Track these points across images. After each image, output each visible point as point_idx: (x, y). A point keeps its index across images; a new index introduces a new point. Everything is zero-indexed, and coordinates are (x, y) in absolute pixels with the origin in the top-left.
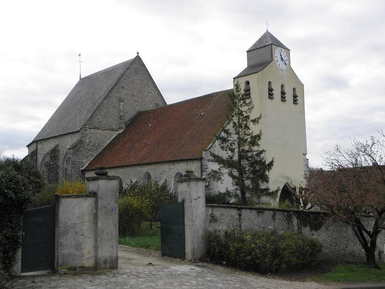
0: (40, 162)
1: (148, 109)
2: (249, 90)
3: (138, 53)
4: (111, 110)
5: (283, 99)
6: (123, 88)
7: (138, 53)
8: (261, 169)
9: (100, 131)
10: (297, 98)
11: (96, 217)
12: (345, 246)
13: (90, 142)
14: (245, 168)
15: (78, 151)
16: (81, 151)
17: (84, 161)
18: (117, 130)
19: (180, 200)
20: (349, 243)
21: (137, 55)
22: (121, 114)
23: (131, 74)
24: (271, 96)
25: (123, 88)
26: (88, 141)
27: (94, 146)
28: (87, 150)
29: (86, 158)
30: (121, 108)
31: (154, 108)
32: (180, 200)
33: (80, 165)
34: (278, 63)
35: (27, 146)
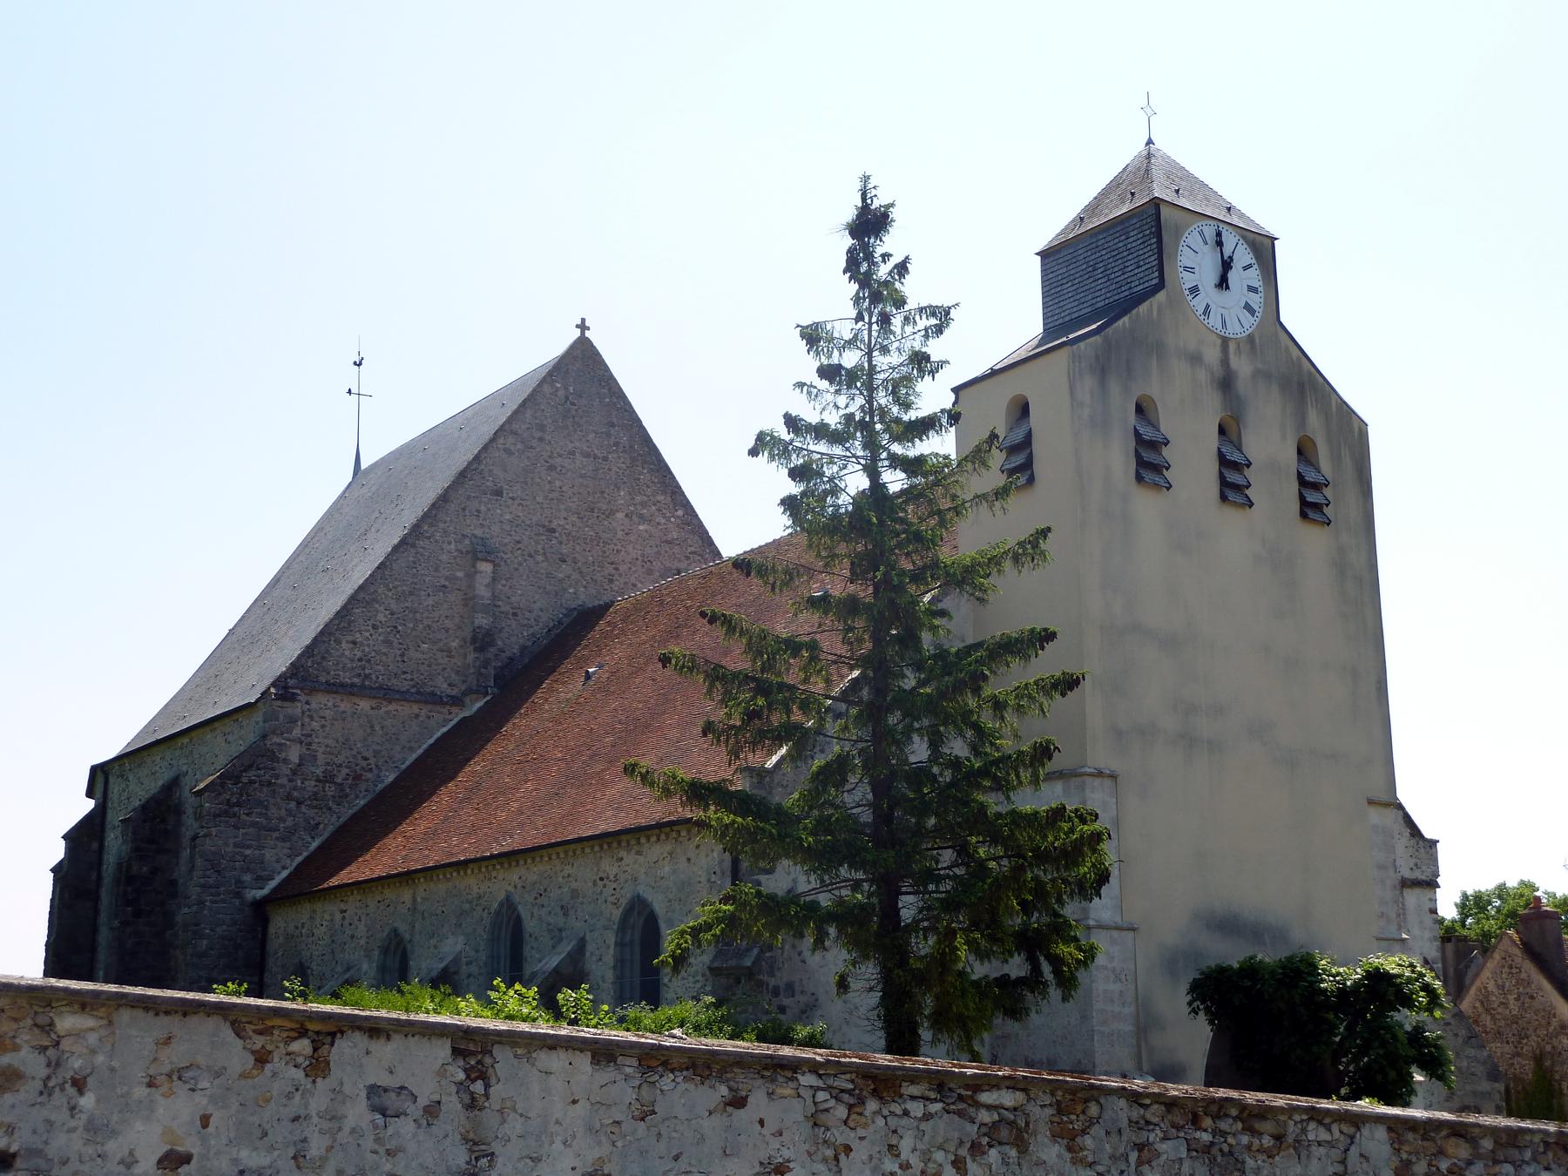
0: (111, 870)
2: (1027, 442)
3: (583, 326)
4: (430, 601)
5: (1232, 483)
6: (499, 493)
7: (583, 326)
9: (364, 705)
10: (1165, 451)
14: (840, 902)
15: (238, 804)
16: (260, 803)
17: (269, 855)
18: (457, 701)
21: (578, 333)
22: (482, 621)
23: (542, 428)
24: (1150, 462)
25: (499, 493)
26: (294, 754)
27: (328, 778)
28: (289, 797)
30: (482, 591)
33: (247, 878)
34: (1198, 304)
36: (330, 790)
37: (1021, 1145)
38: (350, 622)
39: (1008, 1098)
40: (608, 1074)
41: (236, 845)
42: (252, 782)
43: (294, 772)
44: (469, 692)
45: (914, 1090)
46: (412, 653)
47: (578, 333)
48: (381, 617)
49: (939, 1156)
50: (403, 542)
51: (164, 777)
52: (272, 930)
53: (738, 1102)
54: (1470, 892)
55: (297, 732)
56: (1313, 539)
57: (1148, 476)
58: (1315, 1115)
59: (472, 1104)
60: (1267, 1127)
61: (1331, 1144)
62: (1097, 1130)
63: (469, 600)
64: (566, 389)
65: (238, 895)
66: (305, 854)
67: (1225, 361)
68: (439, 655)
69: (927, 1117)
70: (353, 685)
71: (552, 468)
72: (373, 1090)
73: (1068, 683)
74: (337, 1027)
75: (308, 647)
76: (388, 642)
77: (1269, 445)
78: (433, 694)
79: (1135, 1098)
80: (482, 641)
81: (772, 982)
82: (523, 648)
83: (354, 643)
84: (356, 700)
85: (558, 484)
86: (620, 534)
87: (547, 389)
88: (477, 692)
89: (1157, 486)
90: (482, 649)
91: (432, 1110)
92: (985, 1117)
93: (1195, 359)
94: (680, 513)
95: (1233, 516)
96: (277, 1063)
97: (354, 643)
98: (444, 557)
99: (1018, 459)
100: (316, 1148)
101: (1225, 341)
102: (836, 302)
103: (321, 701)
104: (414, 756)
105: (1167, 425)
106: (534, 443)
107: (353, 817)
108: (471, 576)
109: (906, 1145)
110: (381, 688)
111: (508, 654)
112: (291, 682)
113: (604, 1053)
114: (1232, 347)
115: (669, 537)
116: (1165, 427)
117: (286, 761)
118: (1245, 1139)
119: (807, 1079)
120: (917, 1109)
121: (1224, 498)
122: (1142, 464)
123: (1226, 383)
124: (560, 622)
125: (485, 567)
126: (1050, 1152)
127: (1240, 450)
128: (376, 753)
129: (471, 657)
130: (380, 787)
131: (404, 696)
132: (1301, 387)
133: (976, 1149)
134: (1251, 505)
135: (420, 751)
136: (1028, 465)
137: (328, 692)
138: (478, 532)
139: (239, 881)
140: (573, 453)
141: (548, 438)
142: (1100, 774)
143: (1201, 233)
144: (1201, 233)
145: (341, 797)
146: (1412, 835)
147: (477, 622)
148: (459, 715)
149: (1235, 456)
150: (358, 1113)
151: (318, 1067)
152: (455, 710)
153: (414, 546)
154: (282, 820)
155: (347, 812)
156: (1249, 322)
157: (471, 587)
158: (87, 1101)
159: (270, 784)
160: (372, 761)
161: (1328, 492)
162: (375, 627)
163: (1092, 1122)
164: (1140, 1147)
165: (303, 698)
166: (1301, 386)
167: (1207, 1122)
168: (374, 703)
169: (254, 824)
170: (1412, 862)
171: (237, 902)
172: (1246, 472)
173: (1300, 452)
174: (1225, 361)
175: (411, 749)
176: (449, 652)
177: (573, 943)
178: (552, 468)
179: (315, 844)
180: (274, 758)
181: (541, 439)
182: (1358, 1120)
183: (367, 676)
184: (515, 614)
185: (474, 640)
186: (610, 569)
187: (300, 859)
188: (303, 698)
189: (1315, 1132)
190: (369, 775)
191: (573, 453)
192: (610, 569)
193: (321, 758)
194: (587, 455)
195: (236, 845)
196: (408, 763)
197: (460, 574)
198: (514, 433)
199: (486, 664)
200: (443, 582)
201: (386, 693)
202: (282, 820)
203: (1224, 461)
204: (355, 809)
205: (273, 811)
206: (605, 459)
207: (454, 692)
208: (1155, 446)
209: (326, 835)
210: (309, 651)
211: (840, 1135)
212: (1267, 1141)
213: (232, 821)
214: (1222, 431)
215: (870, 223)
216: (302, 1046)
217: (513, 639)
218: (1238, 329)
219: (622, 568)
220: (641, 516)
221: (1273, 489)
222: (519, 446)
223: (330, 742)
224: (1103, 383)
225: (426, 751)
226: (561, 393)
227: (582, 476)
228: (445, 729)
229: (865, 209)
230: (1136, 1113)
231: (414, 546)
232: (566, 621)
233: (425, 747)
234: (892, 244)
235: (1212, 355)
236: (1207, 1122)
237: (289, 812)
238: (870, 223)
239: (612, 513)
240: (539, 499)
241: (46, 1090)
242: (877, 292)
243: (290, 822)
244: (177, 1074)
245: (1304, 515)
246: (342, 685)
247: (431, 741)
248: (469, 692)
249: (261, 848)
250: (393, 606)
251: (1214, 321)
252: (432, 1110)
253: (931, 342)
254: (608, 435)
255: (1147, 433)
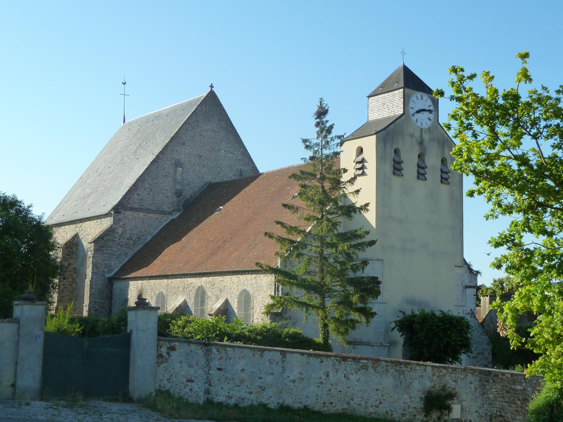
1: (226, 179)
3: (212, 86)
4: (162, 180)
5: (421, 175)
6: (184, 144)
7: (212, 86)
8: (370, 287)
9: (142, 214)
10: (402, 165)
11: (17, 344)
12: (378, 402)
13: (124, 232)
15: (103, 247)
16: (110, 246)
17: (113, 263)
18: (170, 213)
19: (128, 331)
20: (385, 398)
22: (179, 187)
25: (184, 144)
28: (119, 245)
29: (117, 258)
30: (179, 177)
31: (234, 178)
32: (128, 331)
33: (106, 270)
35: (406, 70)
36: (131, 242)
37: (367, 369)
38: (137, 187)
39: (365, 361)
40: (303, 357)
41: (103, 260)
42: (107, 240)
43: (120, 236)
44: (174, 210)
45: (350, 360)
46: (156, 197)
47: (209, 89)
48: (147, 186)
49: (353, 371)
50: (154, 161)
51: (73, 233)
52: (114, 287)
53: (322, 362)
54: (497, 279)
55: (121, 224)
56: (444, 188)
57: (397, 172)
58: (418, 365)
59: (283, 362)
60: (409, 366)
61: (421, 370)
62: (379, 367)
63: (175, 180)
64: (206, 108)
65: (103, 275)
66: (123, 263)
67: (421, 136)
68: (165, 198)
69: (351, 364)
70: (138, 208)
71: (201, 135)
72: (269, 360)
73: (372, 243)
74: (264, 350)
75: (124, 196)
76: (148, 194)
77: (433, 161)
78: (163, 211)
79: (386, 361)
80: (179, 194)
81: (286, 316)
82: (191, 196)
83: (138, 194)
84: (139, 213)
85: (203, 141)
86: (222, 158)
87: (200, 108)
88: (177, 211)
89: (399, 175)
90: (178, 197)
91: (277, 363)
92: (361, 364)
93: (412, 136)
94: (242, 150)
95: (421, 183)
96: (256, 355)
97: (138, 194)
98: (166, 166)
99: (359, 166)
100: (261, 369)
101: (422, 129)
102: (312, 133)
103: (128, 213)
104: (157, 231)
105: (403, 157)
106: (196, 127)
107: (139, 251)
108: (175, 172)
109: (348, 369)
110: (147, 209)
111: (186, 198)
112: (119, 207)
113: (302, 354)
114: (424, 131)
115: (238, 158)
116: (402, 157)
117: (118, 233)
118: (405, 369)
119: (333, 358)
120: (350, 363)
121: (418, 178)
122: (395, 168)
123: (421, 143)
124: (203, 187)
125: (180, 169)
126: (371, 370)
127: (424, 162)
128: (145, 230)
129: (175, 199)
130: (147, 241)
131: (154, 212)
132: (444, 142)
133: (359, 370)
134: (426, 179)
135: (159, 230)
136: (362, 168)
137: (130, 210)
138: (177, 157)
139: (103, 271)
140: (208, 130)
141: (200, 125)
142: (378, 260)
143: (416, 97)
144: (416, 97)
145: (135, 244)
146: (470, 272)
147: (177, 188)
148: (171, 218)
149: (422, 165)
150: (267, 363)
151: (262, 356)
152: (169, 216)
153: (157, 162)
154: (116, 252)
155: (136, 249)
156: (429, 123)
157: (175, 175)
158: (231, 361)
159: (113, 240)
160: (144, 233)
161: (449, 174)
162: (145, 189)
163: (379, 365)
164: (387, 370)
165: (123, 212)
166: (444, 142)
167: (398, 366)
168: (144, 214)
169: (108, 253)
170: (469, 280)
171: (103, 277)
172: (426, 170)
173: (442, 161)
174: (421, 136)
175: (156, 229)
176: (168, 197)
177: (224, 300)
178: (201, 135)
179: (126, 260)
180: (114, 232)
181: (198, 126)
182: (426, 366)
183: (142, 205)
184: (189, 185)
185: (176, 193)
186: (219, 169)
187: (122, 264)
188: (123, 212)
189: (418, 368)
190: (143, 237)
191: (208, 130)
192: (219, 169)
193: (128, 232)
194: (212, 131)
195: (103, 260)
196: (155, 234)
197: (171, 171)
198: (189, 124)
199: (180, 201)
200: (166, 174)
201: (148, 211)
202: (116, 252)
203: (419, 166)
204: (139, 248)
205: (114, 249)
206: (218, 132)
207: (169, 210)
208: (400, 163)
209: (130, 257)
210: (124, 197)
211: (338, 367)
212: (409, 369)
213: (101, 252)
214: (419, 156)
215: (322, 113)
216: (259, 353)
217: (188, 193)
218: (426, 126)
219: (223, 169)
220: (229, 151)
221: (433, 174)
222: (191, 128)
223: (131, 227)
224: (385, 145)
225: (161, 230)
226: (204, 110)
227: (211, 138)
228: (166, 223)
229: (321, 107)
230: (386, 364)
231: (157, 162)
232: (205, 187)
233: (160, 228)
234: (330, 119)
235: (417, 134)
236: (398, 366)
237: (119, 250)
238: (322, 113)
239: (220, 150)
240: (197, 146)
241: (226, 360)
242: (325, 130)
243: (119, 252)
244: (243, 357)
245: (442, 182)
246: (135, 208)
247: (162, 226)
248: (174, 210)
249: (110, 261)
250: (150, 182)
251: (419, 124)
252: (277, 363)
253: (365, 271)
254: (219, 124)
255: (397, 159)
